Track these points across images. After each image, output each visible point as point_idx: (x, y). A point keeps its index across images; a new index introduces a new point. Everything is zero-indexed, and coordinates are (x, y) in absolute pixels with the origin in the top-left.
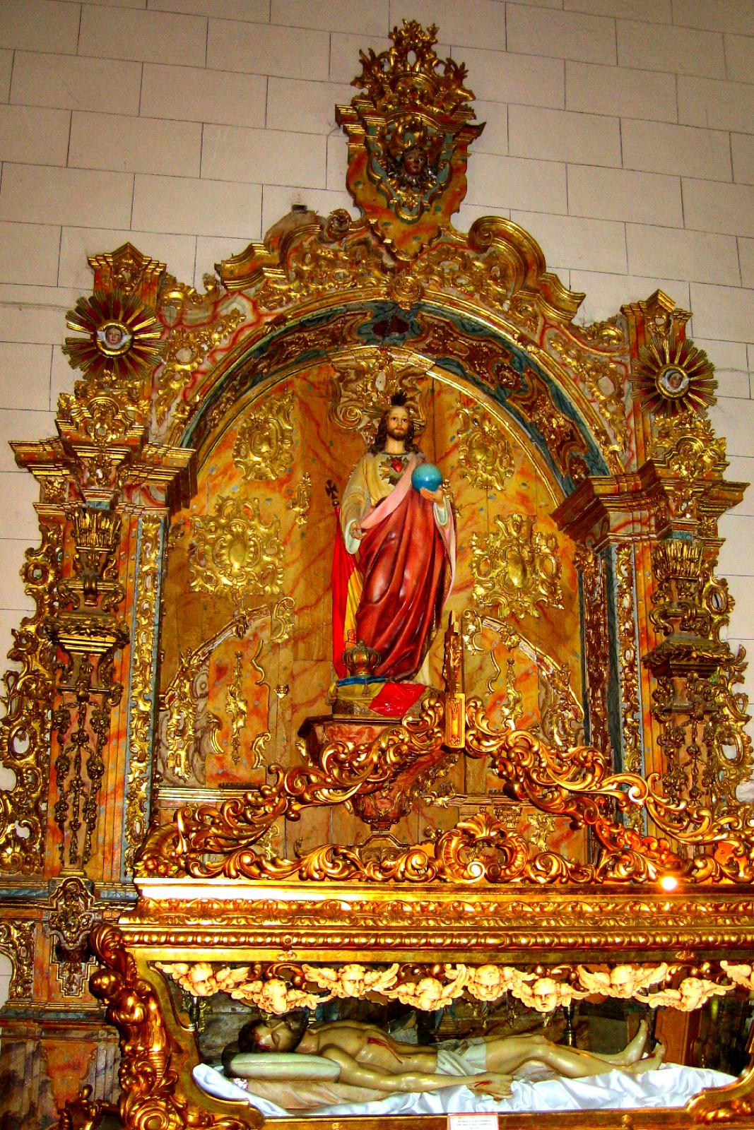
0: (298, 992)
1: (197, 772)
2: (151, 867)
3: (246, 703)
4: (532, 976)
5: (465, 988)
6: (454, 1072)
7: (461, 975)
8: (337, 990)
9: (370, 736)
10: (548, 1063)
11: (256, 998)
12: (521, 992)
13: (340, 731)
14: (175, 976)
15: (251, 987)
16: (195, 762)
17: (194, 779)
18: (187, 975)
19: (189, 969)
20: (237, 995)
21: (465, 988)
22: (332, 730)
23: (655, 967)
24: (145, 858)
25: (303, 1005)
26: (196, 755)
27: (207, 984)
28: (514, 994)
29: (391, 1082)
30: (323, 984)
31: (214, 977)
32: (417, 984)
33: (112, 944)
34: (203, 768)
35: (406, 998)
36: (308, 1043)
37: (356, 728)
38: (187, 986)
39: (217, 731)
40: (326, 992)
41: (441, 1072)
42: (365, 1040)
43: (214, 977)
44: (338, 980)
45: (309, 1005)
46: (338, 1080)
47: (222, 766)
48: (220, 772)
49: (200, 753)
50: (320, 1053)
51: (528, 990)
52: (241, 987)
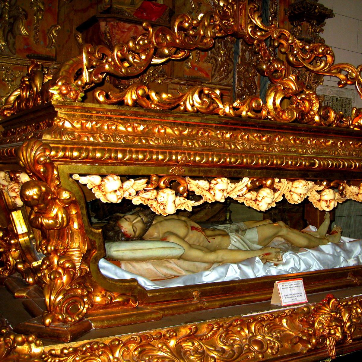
0: (182, 198)
1: (10, 46)
2: (65, 92)
3: (43, 4)
4: (321, 188)
5: (283, 196)
6: (241, 247)
7: (283, 185)
8: (209, 197)
9: (135, 32)
10: (287, 241)
11: (149, 203)
12: (314, 197)
13: (118, 26)
14: (89, 187)
15: (146, 195)
16: (9, 39)
17: (8, 50)
18: (99, 186)
19: (102, 181)
20: (136, 201)
21: (283, 196)
22: (112, 25)
23: (238, 182)
24: (60, 83)
25: (183, 209)
26: (10, 34)
27: (118, 193)
28: (309, 199)
29: (212, 257)
30: (198, 192)
31: (121, 188)
32: (258, 193)
33: (42, 159)
34: (14, 44)
35: (248, 202)
36: (153, 232)
37: (128, 25)
38: (98, 195)
39: (24, 21)
40: (200, 197)
41: (233, 248)
42: (190, 228)
43: (121, 188)
44: (209, 190)
45: (187, 209)
46: (181, 258)
47: (27, 44)
48: (26, 47)
49: (12, 34)
50: (163, 239)
51: (318, 197)
52: (141, 195)
